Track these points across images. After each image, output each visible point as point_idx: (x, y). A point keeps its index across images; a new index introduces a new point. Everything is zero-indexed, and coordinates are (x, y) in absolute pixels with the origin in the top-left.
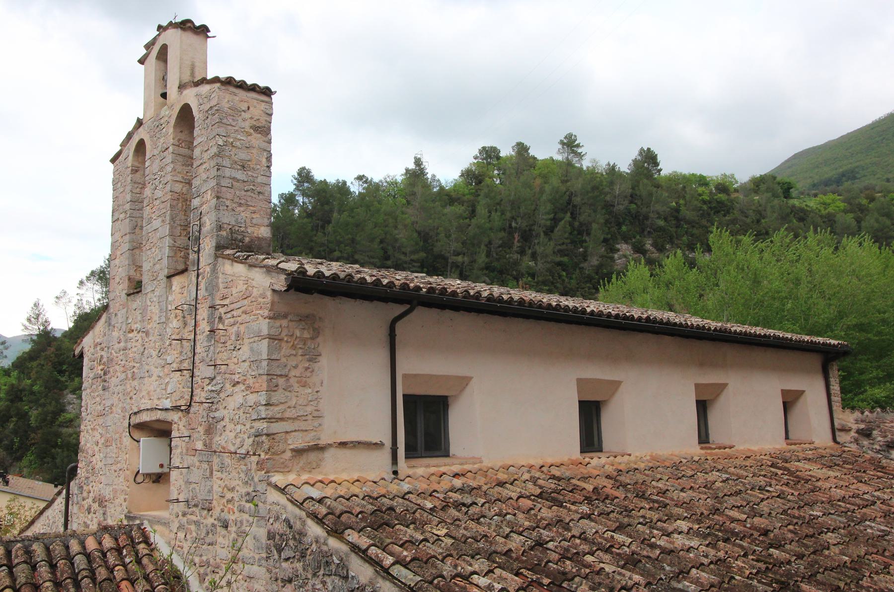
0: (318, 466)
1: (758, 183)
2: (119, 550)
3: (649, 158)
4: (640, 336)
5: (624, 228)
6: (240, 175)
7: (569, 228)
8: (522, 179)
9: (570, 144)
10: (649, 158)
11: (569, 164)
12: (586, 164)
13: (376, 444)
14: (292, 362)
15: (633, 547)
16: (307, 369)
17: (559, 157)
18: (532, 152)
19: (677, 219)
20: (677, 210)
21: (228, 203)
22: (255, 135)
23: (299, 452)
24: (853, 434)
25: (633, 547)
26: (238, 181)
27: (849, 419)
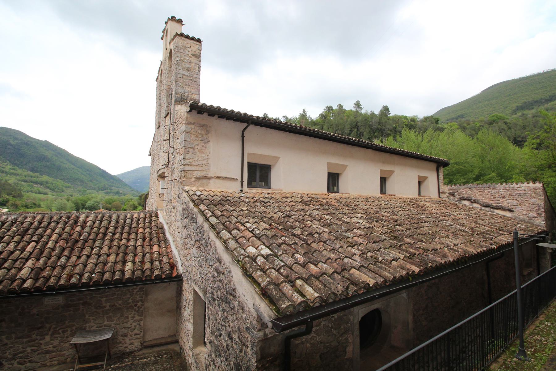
0: (207, 185)
1: (426, 119)
2: (145, 219)
3: (386, 109)
4: (357, 148)
5: (376, 134)
6: (186, 73)
7: (356, 134)
8: (340, 116)
9: (358, 104)
10: (386, 109)
11: (357, 112)
12: (363, 112)
13: (233, 179)
14: (196, 143)
15: (332, 221)
16: (203, 146)
17: (354, 109)
18: (344, 107)
19: (395, 131)
20: (396, 128)
21: (180, 84)
22: (193, 58)
23: (198, 179)
24: (447, 194)
25: (332, 221)
26: (185, 76)
27: (446, 189)
